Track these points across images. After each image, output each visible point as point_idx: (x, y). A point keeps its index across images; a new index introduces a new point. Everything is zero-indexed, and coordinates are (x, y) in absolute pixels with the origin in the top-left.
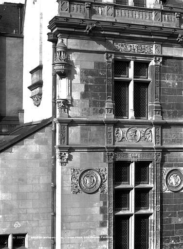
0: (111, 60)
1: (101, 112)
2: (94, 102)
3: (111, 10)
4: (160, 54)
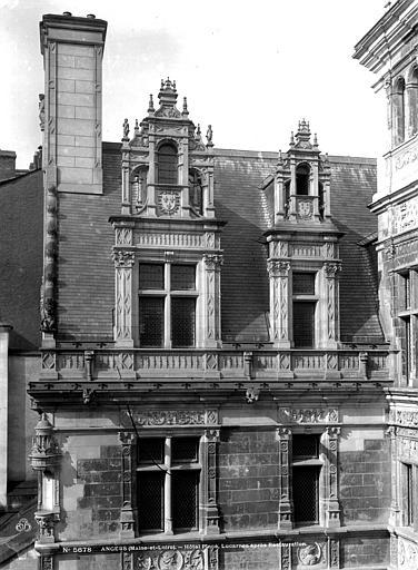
0: (286, 437)
1: (113, 528)
2: (100, 512)
3: (334, 360)
4: (337, 423)
